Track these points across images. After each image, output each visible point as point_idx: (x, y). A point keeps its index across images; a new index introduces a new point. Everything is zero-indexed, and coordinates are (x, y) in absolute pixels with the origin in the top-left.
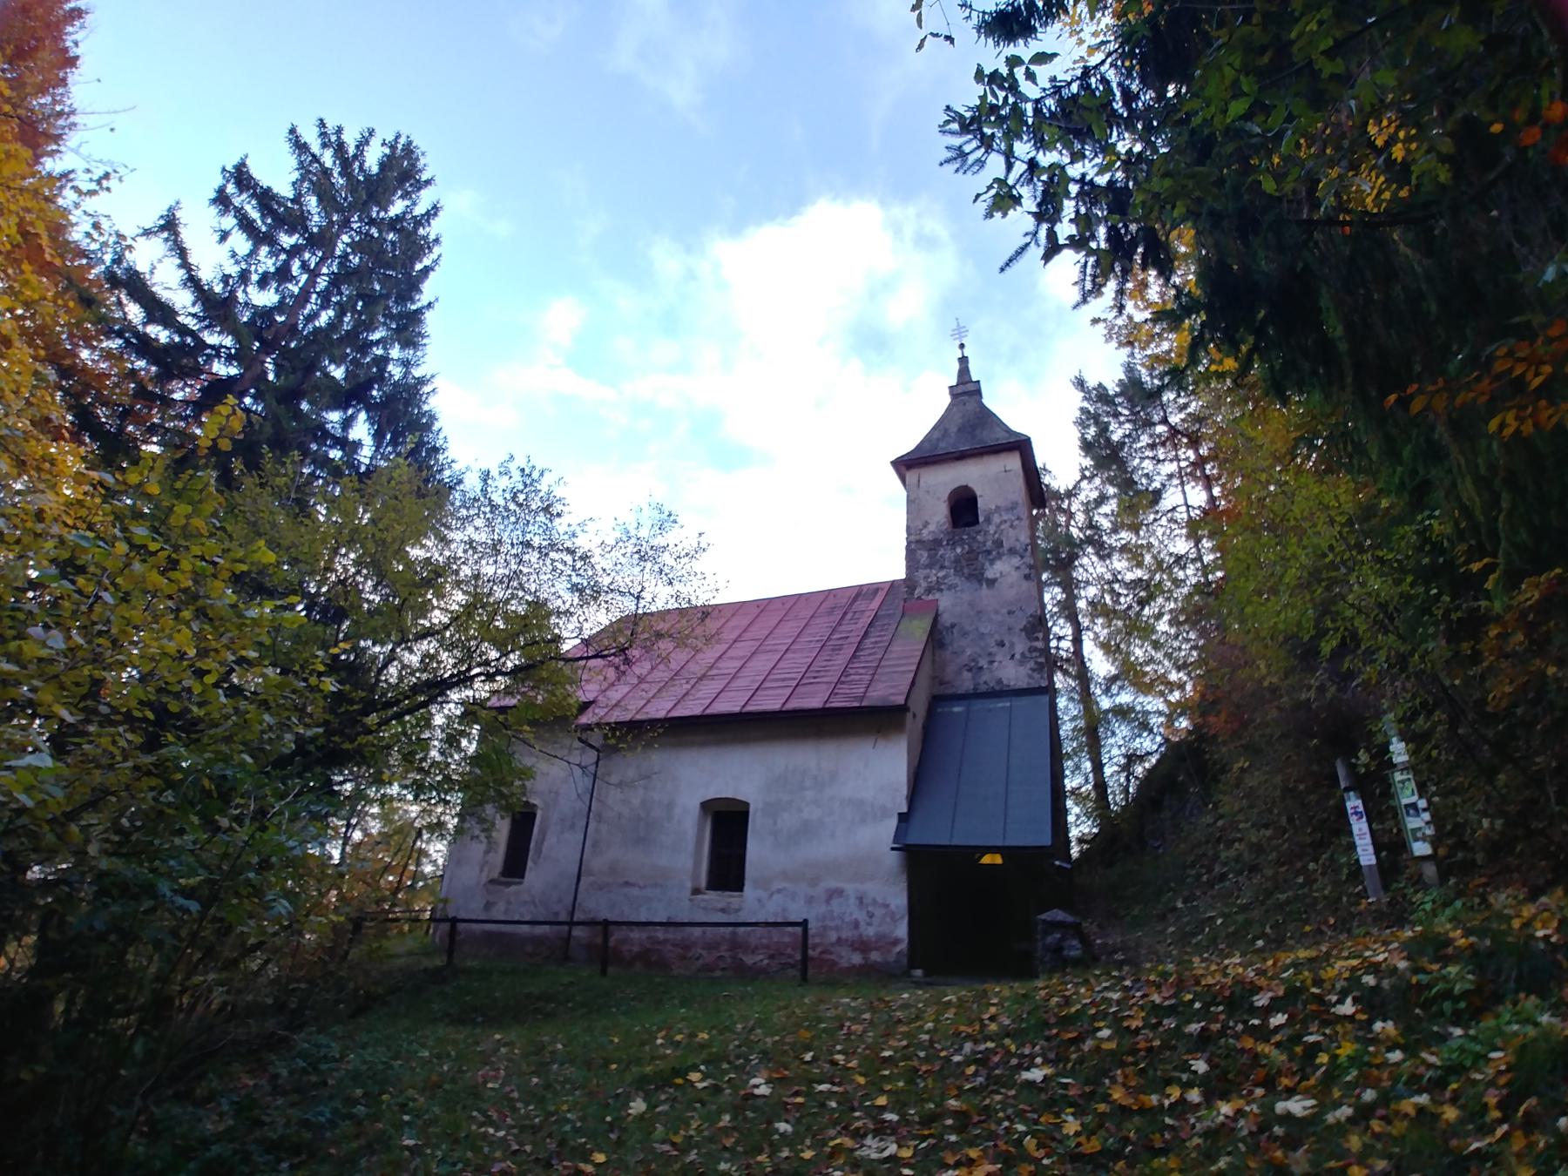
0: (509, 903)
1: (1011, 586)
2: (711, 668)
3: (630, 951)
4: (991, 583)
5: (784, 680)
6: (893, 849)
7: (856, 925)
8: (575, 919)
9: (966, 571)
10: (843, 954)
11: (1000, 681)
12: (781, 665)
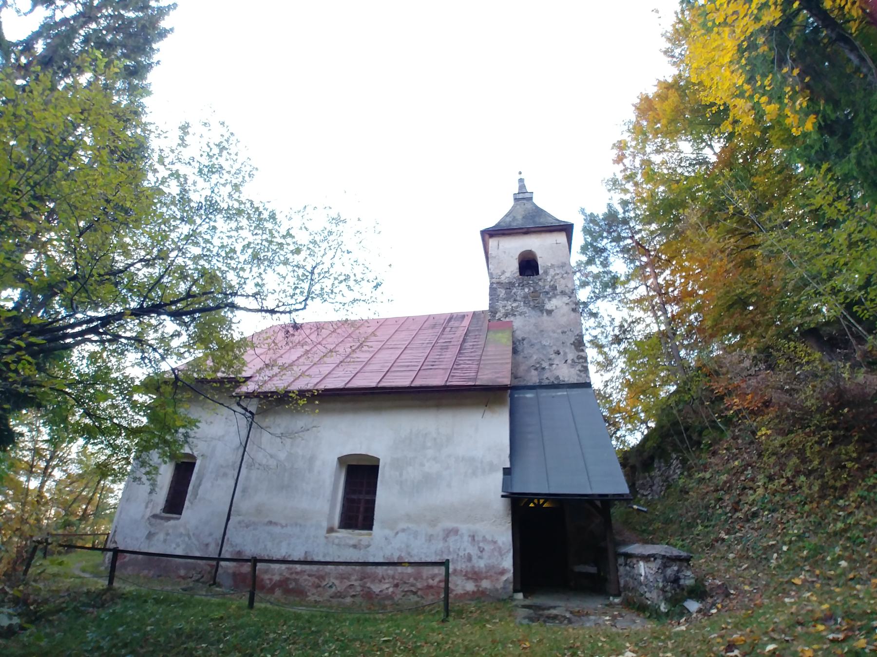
0: (167, 534)
1: (564, 315)
2: (348, 356)
3: (271, 580)
4: (549, 312)
5: (408, 366)
6: (503, 496)
7: (470, 558)
8: (222, 556)
9: (531, 303)
10: (459, 582)
11: (557, 378)
12: (402, 357)
